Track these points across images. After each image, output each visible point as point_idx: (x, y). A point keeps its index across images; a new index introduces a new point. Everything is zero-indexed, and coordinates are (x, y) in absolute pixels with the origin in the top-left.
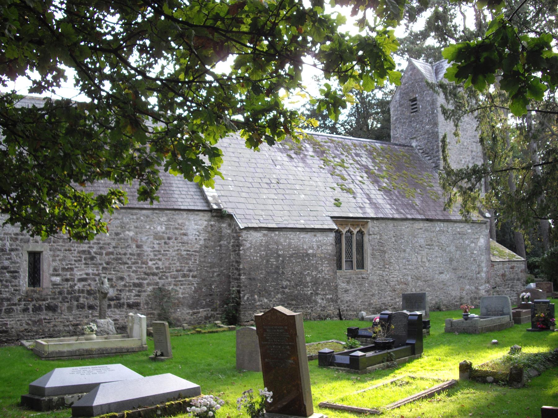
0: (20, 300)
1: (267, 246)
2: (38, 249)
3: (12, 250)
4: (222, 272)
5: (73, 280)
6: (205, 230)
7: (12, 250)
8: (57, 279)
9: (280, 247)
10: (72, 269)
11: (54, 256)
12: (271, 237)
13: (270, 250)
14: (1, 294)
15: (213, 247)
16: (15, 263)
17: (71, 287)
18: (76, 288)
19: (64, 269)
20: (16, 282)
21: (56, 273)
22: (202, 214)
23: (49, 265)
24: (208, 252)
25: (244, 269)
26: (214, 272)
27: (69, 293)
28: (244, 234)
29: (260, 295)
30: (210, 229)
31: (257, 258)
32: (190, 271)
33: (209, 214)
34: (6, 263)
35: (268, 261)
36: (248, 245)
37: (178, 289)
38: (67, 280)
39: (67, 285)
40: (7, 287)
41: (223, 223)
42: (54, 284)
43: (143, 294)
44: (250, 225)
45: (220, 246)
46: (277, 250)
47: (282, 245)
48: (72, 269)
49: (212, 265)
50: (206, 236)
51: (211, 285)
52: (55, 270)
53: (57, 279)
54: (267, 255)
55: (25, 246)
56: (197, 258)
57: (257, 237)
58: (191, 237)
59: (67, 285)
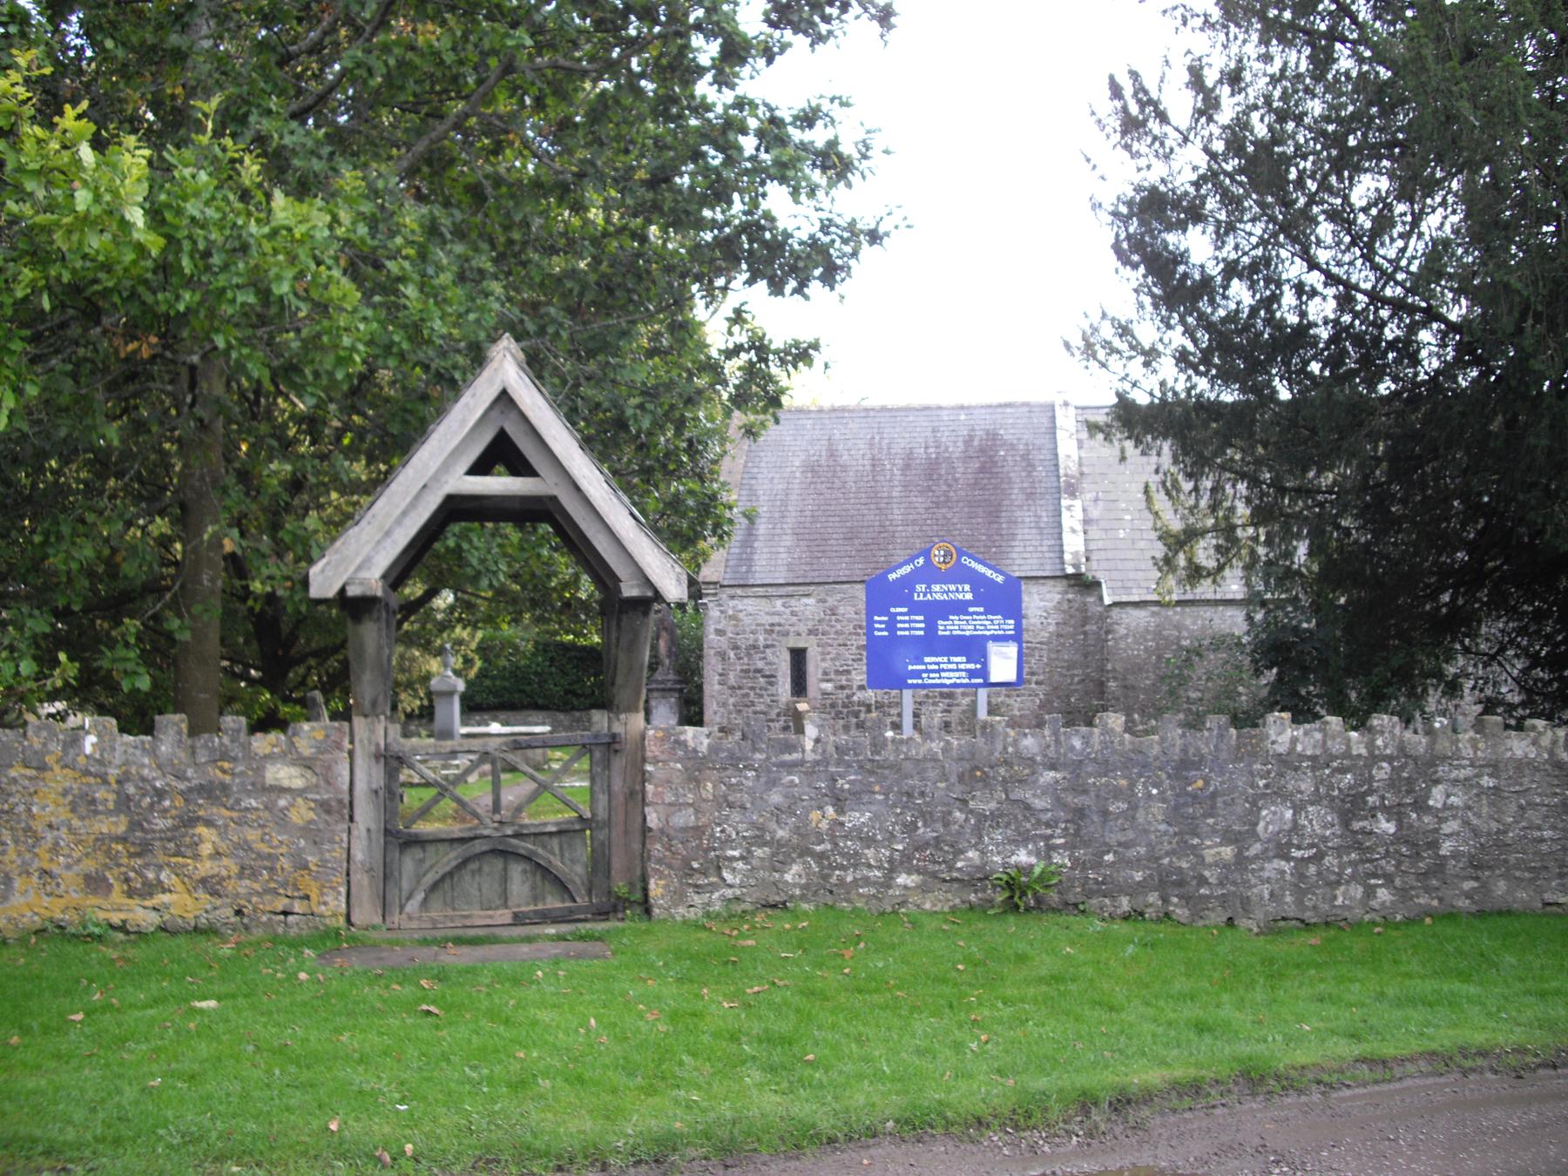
0: (778, 715)
1: (1158, 633)
2: (801, 645)
3: (767, 646)
4: (1088, 675)
5: (851, 687)
6: (1057, 608)
7: (767, 646)
8: (828, 686)
9: (1185, 634)
10: (848, 672)
11: (823, 653)
12: (1167, 617)
13: (1166, 638)
14: (118, 3)
15: (1073, 636)
16: (770, 664)
17: (848, 697)
18: (855, 698)
19: (837, 672)
20: (772, 690)
21: (499, 484)
22: (1052, 582)
23: (817, 666)
24: (1063, 644)
25: (1114, 670)
26: (1073, 676)
27: (845, 706)
28: (1115, 612)
29: (1142, 712)
30: (1065, 606)
31: (1138, 651)
32: (1033, 674)
33: (1065, 582)
34: (760, 664)
35: (1160, 657)
36: (1123, 631)
37: (1011, 701)
38: (842, 688)
39: (842, 694)
40: (761, 696)
41: (1090, 595)
42: (825, 693)
43: (955, 709)
44: (1125, 599)
45: (1085, 633)
46: (1179, 638)
47: (1187, 629)
48: (848, 672)
49: (1071, 665)
50: (1058, 617)
51: (1068, 697)
52: (825, 673)
53: (828, 686)
54: (1158, 648)
55: (784, 640)
56: (1045, 653)
57: (1140, 617)
58: (1033, 621)
59: (842, 694)
